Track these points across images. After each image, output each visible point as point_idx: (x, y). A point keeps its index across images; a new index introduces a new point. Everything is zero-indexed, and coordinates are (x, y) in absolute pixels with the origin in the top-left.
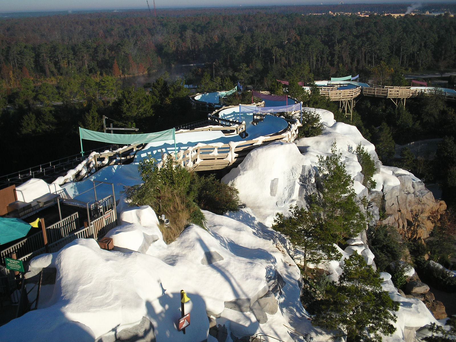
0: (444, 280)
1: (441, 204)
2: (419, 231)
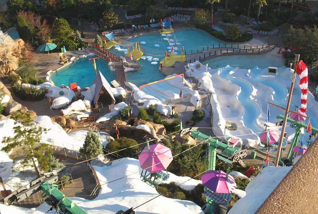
0: (34, 94)
1: (19, 42)
2: (10, 65)
